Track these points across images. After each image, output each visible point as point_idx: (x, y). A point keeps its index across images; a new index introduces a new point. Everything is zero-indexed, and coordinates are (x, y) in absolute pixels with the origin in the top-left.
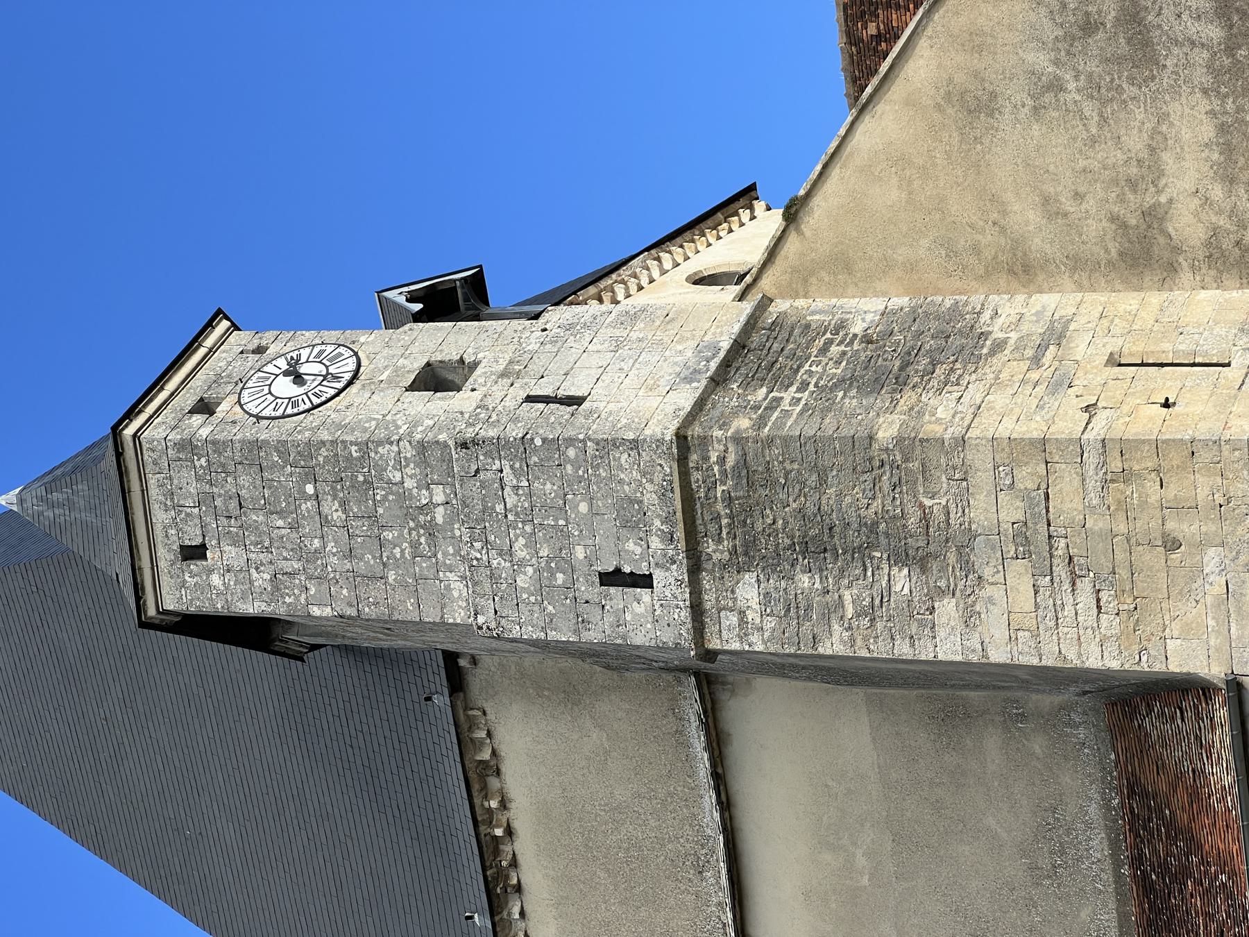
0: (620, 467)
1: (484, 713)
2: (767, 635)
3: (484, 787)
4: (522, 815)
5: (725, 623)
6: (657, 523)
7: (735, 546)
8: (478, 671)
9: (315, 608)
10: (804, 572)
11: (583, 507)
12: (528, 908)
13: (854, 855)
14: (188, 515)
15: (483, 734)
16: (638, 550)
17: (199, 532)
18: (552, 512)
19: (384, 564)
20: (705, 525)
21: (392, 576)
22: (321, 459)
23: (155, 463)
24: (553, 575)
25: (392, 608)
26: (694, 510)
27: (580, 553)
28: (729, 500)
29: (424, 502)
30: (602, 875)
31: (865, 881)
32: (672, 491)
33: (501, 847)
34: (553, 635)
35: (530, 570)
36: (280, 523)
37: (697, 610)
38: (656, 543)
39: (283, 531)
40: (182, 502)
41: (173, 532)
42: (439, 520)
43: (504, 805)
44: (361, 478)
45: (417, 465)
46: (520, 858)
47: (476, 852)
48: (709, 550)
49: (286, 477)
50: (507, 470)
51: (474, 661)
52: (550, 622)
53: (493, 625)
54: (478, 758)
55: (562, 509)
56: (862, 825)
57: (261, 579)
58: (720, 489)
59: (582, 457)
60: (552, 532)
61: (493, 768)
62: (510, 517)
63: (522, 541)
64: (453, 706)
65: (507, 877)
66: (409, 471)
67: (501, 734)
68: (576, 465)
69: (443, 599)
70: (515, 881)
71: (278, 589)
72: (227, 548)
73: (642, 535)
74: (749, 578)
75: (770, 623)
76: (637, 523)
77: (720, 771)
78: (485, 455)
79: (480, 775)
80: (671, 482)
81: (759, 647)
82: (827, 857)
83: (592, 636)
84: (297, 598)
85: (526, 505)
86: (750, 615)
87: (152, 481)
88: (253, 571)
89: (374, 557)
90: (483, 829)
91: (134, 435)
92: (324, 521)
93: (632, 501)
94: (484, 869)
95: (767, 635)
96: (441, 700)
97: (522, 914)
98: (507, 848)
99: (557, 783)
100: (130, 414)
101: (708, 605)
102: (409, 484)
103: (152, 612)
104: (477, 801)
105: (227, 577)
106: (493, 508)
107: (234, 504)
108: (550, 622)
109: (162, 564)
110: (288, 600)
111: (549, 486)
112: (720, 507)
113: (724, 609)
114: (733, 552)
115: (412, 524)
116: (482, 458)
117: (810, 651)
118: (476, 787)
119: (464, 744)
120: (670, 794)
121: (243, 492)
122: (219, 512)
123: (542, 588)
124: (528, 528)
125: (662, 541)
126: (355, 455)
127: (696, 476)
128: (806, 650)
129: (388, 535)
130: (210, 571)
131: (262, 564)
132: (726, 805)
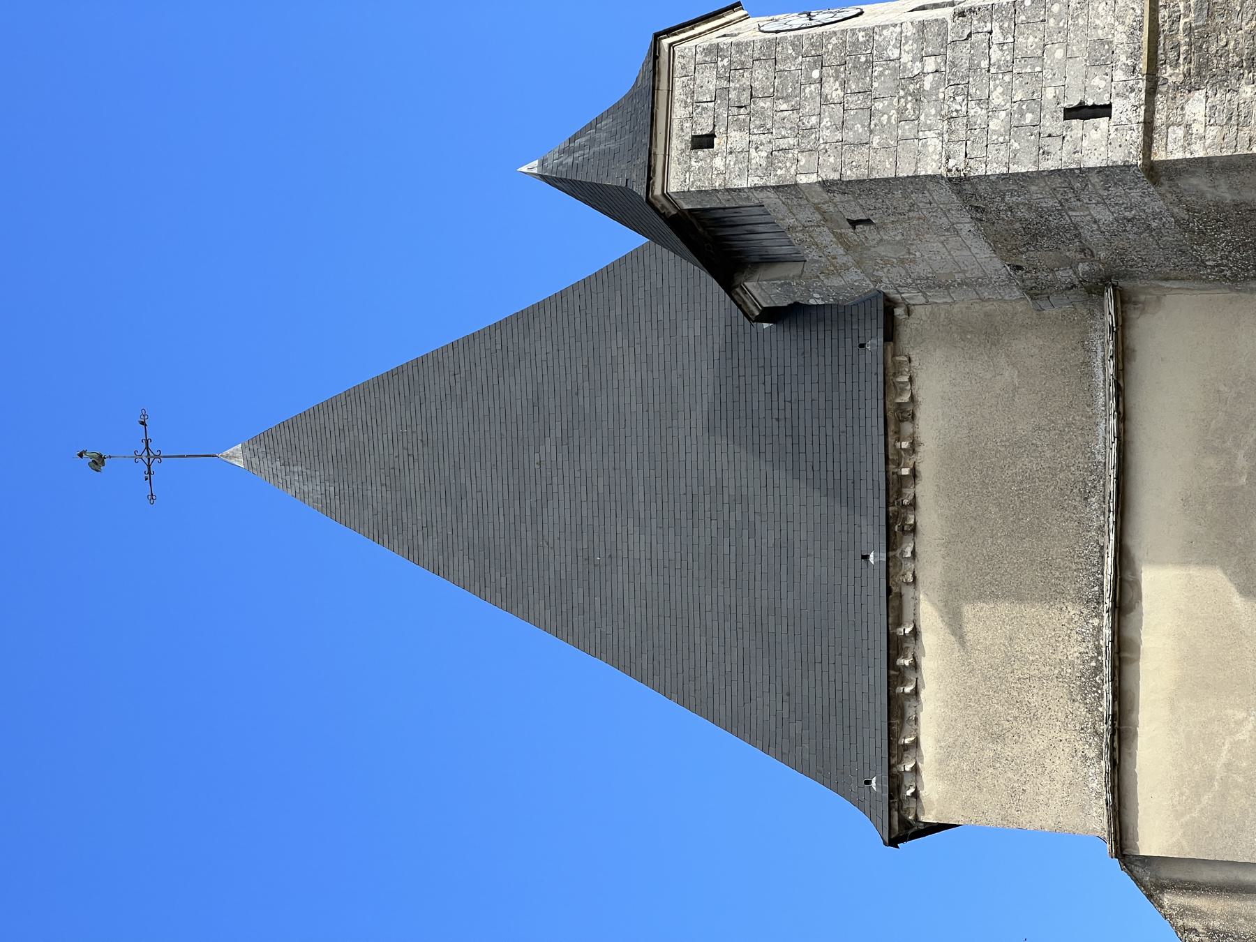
0: (1098, 15)
1: (910, 360)
2: (1208, 142)
3: (898, 432)
4: (928, 461)
5: (1171, 136)
6: (1123, 58)
7: (1189, 69)
8: (911, 321)
9: (803, 177)
10: (1247, 84)
11: (1059, 54)
12: (919, 550)
13: (1235, 457)
14: (704, 109)
15: (906, 379)
16: (1102, 84)
17: (710, 122)
18: (1030, 61)
19: (871, 132)
20: (1165, 54)
21: (876, 141)
22: (830, 47)
23: (683, 67)
24: (1022, 115)
25: (870, 169)
26: (1157, 42)
27: (1050, 93)
28: (1189, 30)
29: (916, 72)
30: (993, 509)
31: (1243, 480)
32: (1141, 29)
33: (904, 490)
34: (1014, 169)
35: (1003, 114)
36: (784, 107)
37: (1149, 127)
38: (1119, 75)
39: (786, 113)
40: (700, 99)
41: (688, 125)
42: (927, 86)
43: (913, 449)
44: (863, 59)
45: (915, 41)
46: (920, 501)
47: (883, 487)
48: (1165, 76)
49: (796, 66)
50: (996, 30)
51: (909, 312)
52: (1014, 157)
53: (962, 166)
54: (898, 400)
55: (1041, 58)
56: (1247, 427)
57: (759, 157)
58: (1182, 22)
59: (1064, 10)
60: (1027, 78)
61: (906, 414)
62: (993, 70)
63: (1000, 89)
64: (885, 350)
65: (905, 519)
66: (907, 48)
67: (918, 382)
68: (1058, 18)
69: (919, 155)
70: (912, 522)
71: (772, 164)
72: (733, 134)
73: (1108, 70)
74: (1199, 95)
75: (1213, 132)
76: (1105, 61)
77: (1121, 382)
78: (979, 20)
79: (899, 416)
80: (1141, 22)
81: (1200, 154)
82: (1211, 461)
83: (1049, 164)
84: (788, 170)
85: (1008, 58)
86: (1195, 127)
87: (678, 83)
88: (752, 150)
89: (863, 126)
90: (892, 467)
91: (670, 45)
92: (824, 100)
93: (1102, 42)
94: (887, 506)
95: (1208, 142)
96: (875, 343)
97: (913, 552)
98: (909, 492)
99: (965, 424)
100: (669, 32)
101: (1158, 123)
102: (906, 58)
103: (658, 192)
104: (891, 440)
105: (729, 158)
106: (979, 64)
107: (746, 94)
108: (1014, 157)
109: (674, 154)
110: (779, 172)
111: (1031, 39)
112: (1182, 38)
113: (1173, 124)
114: (1188, 74)
115: (902, 93)
116: (975, 22)
117: (1246, 152)
118: (892, 427)
119: (888, 386)
120: (1069, 425)
121: (756, 84)
122: (732, 103)
123: (1012, 129)
124: (1007, 78)
125: (1125, 74)
126: (861, 39)
127: (1163, 13)
128: (1242, 151)
129: (879, 105)
130: (715, 155)
131: (762, 144)
132: (1123, 417)
